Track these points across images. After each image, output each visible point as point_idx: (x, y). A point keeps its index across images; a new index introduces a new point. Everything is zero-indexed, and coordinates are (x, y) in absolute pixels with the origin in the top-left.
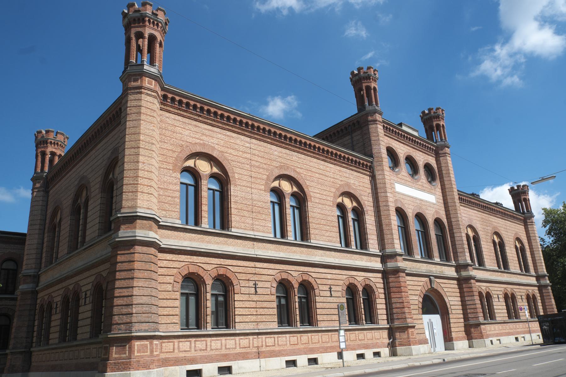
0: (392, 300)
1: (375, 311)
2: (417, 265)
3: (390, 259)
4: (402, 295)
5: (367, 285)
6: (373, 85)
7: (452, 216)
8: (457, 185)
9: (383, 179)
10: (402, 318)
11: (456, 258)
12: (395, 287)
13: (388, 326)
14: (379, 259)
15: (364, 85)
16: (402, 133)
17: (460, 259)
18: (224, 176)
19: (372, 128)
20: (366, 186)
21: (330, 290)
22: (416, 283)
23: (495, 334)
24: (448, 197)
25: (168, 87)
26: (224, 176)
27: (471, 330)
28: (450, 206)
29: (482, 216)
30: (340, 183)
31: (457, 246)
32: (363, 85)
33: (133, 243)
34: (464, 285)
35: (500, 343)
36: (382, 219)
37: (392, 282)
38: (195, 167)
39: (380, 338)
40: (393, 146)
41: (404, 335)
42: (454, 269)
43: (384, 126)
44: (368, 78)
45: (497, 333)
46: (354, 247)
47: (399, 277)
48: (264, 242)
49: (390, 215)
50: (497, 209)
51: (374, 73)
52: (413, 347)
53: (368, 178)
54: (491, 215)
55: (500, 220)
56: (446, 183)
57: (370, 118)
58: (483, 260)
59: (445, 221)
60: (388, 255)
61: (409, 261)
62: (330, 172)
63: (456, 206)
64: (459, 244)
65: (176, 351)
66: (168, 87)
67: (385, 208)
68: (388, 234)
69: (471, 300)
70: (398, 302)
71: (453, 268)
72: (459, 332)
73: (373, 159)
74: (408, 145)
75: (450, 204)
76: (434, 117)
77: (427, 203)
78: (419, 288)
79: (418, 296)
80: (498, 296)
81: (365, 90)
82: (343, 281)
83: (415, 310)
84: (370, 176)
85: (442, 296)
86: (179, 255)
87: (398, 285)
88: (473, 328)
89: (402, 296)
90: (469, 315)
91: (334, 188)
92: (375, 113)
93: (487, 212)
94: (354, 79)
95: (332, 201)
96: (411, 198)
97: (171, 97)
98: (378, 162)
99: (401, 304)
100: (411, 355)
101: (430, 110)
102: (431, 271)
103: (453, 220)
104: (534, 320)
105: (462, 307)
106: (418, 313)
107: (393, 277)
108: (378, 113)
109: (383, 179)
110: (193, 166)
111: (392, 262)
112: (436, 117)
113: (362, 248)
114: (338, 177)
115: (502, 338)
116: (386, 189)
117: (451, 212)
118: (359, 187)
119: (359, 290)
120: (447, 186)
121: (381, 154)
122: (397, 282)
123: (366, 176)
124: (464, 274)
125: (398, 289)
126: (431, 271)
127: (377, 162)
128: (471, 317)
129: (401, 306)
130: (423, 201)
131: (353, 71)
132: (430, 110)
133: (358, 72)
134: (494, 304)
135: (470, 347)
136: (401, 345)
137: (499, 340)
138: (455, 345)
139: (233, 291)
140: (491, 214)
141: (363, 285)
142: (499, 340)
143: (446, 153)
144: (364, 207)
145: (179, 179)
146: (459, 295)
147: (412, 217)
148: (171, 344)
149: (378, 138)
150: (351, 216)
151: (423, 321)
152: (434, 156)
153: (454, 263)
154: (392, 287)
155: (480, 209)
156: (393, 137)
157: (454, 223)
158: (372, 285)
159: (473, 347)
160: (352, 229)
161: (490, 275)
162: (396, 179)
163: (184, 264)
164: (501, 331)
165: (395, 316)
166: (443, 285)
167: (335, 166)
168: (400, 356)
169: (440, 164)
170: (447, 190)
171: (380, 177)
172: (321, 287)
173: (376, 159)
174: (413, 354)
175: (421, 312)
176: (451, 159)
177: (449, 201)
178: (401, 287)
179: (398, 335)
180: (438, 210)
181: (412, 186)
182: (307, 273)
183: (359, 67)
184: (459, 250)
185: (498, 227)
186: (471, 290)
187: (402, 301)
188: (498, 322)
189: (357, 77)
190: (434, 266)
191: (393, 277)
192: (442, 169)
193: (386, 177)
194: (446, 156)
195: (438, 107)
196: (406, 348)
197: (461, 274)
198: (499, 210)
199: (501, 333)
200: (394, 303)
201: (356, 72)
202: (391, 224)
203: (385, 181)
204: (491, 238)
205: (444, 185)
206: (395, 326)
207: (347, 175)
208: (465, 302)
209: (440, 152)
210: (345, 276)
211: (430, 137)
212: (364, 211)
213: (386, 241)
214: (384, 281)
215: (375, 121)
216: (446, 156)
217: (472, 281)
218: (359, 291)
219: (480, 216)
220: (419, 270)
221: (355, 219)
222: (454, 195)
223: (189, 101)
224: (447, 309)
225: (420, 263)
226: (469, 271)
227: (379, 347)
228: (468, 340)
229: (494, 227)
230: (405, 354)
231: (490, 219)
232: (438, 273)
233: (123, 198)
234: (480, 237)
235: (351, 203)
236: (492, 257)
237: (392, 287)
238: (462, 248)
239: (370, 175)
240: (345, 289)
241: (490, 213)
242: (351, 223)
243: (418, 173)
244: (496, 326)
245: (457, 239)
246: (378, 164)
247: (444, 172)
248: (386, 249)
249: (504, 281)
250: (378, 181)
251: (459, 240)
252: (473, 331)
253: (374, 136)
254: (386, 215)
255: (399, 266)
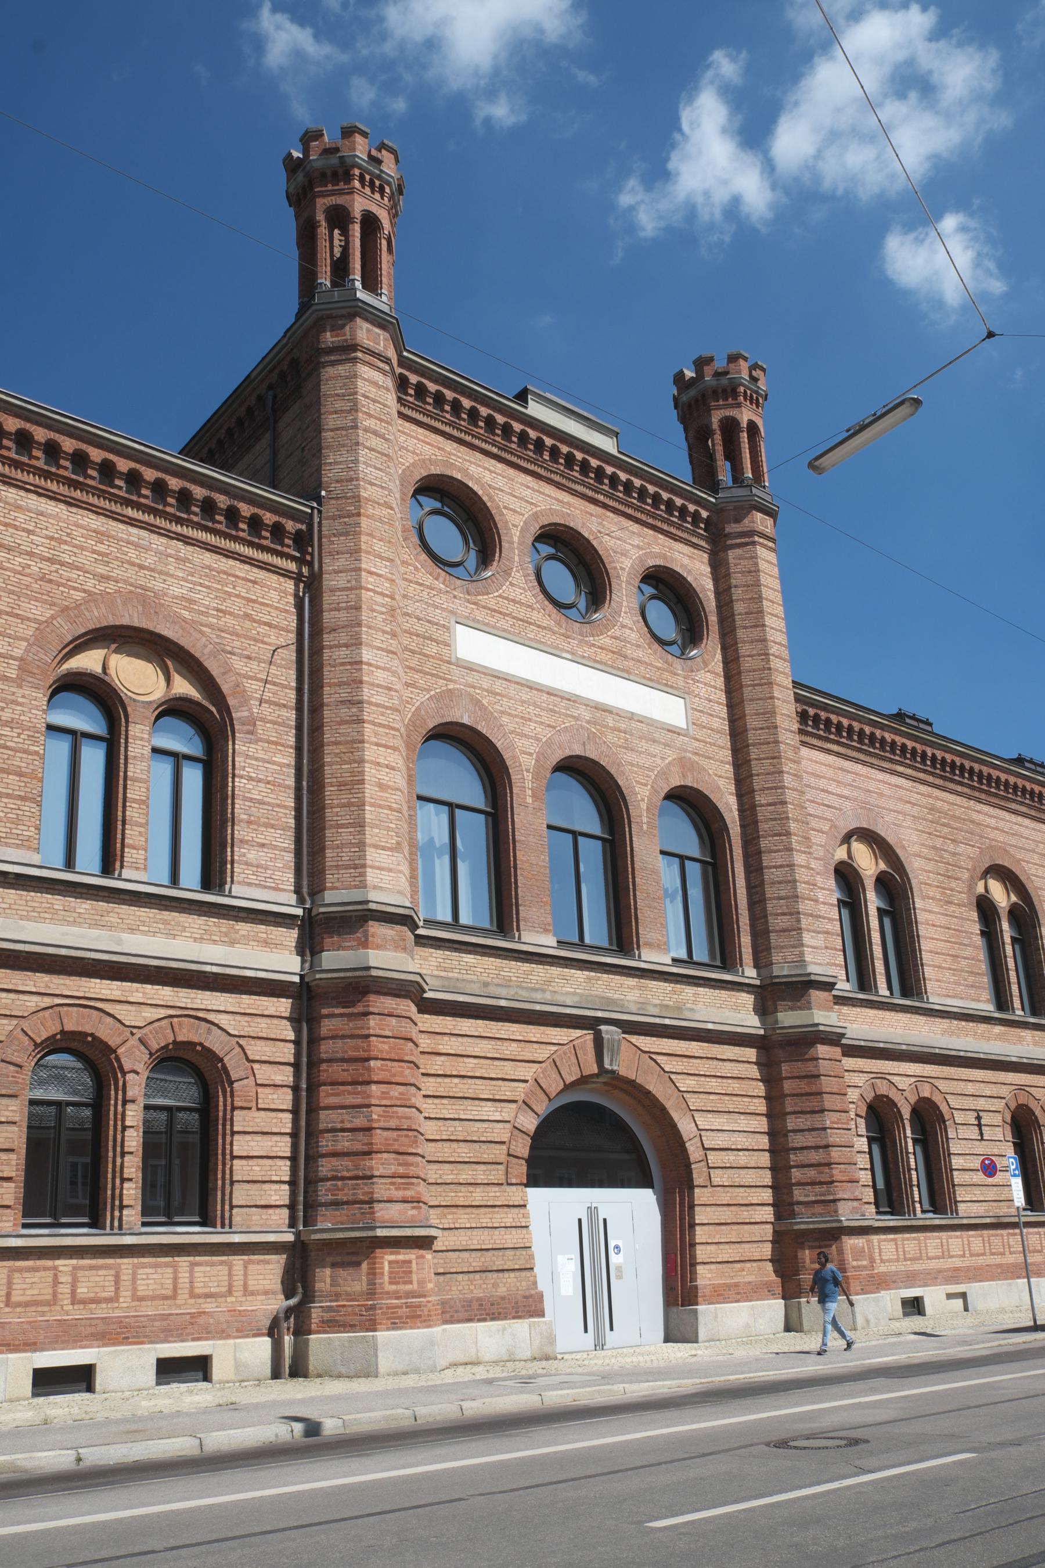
0: (318, 1119)
1: (224, 1164)
2: (527, 974)
3: (339, 934)
4: (369, 1096)
5: (1020, 1106)
6: (745, 415)
7: (757, 783)
8: (793, 661)
9: (350, 589)
10: (355, 1202)
11: (761, 957)
12: (343, 1060)
13: (290, 1237)
14: (290, 936)
15: (716, 418)
16: (575, 452)
17: (776, 957)
18: (213, 709)
19: (336, 378)
20: (267, 618)
21: (979, 1121)
22: (510, 1050)
23: (940, 1271)
24: (749, 708)
25: (142, 448)
26: (213, 709)
27: (800, 1254)
28: (754, 745)
29: (931, 801)
30: (90, 584)
31: (769, 906)
32: (318, 206)
33: (816, 1036)
34: (785, 1069)
35: (966, 1309)
36: (327, 759)
37: (333, 1037)
38: (102, 676)
39: (230, 1292)
40: (472, 478)
41: (355, 1282)
42: (747, 999)
43: (402, 384)
44: (730, 392)
45: (956, 1270)
46: (883, 990)
47: (367, 1014)
48: (262, 922)
49: (362, 742)
50: (1012, 780)
51: (751, 376)
52: (382, 1336)
53: (289, 585)
54: (979, 801)
55: (1027, 822)
56: (744, 649)
57: (329, 338)
58: (917, 971)
59: (728, 803)
60: (329, 918)
61: (484, 954)
62: (29, 532)
63: (777, 742)
64: (780, 898)
65: (125, 1294)
66: (142, 448)
67: (344, 712)
68: (342, 826)
69: (809, 1130)
70: (349, 1126)
71: (744, 995)
72: (738, 1266)
73: (320, 504)
74: (559, 486)
75: (752, 737)
76: (715, 392)
77: (634, 724)
78: (528, 1072)
79: (513, 1106)
80: (979, 1118)
81: (718, 432)
82: (858, 1090)
83: (482, 1167)
84: (298, 578)
85: (663, 1110)
86: (93, 980)
87: (357, 1049)
88: (811, 1248)
89: (366, 1102)
90: (796, 1192)
91: (45, 602)
92: (352, 316)
93: (959, 788)
94: (684, 398)
95: (21, 659)
96: (545, 696)
97: (152, 480)
98: (340, 517)
99: (360, 1136)
100: (369, 1372)
101: (700, 364)
102: (608, 1003)
103: (761, 799)
104: (909, 1223)
105: (773, 1159)
106: (502, 1179)
107: (342, 1015)
108: (366, 320)
109: (350, 589)
110: (98, 669)
111: (344, 949)
112: (724, 391)
113: (905, 993)
114: (85, 559)
115: (974, 1289)
116: (359, 633)
117: (756, 768)
118: (219, 618)
119: (121, 1067)
120: (746, 664)
121: (357, 487)
122: (352, 1037)
123: (275, 577)
124: (788, 1018)
125: (352, 1067)
126: (610, 1001)
127: (334, 518)
128: (802, 1199)
129: (359, 1147)
130: (611, 712)
131: (682, 372)
132: (700, 364)
133: (696, 373)
134: (953, 1150)
135: (788, 1329)
136: (332, 1325)
137: (963, 1296)
138: (702, 1320)
139: (120, 1093)
140: (983, 796)
141: (913, 1099)
142: (963, 1296)
143: (752, 533)
144: (231, 702)
145: (149, 741)
146: (763, 1109)
147: (536, 777)
148: (224, 1270)
149: (355, 420)
150: (873, 901)
151: (526, 1216)
152: (703, 543)
153: (750, 974)
154: (330, 1061)
155: (925, 771)
156: (477, 442)
157: (762, 813)
158: (216, 1048)
159: (801, 1331)
160: (876, 937)
161: (944, 1032)
162: (464, 609)
163: (163, 1012)
164: (981, 1261)
165: (324, 1192)
166: (669, 1065)
167: (74, 510)
168: (319, 1376)
169: (728, 575)
170: (746, 680)
171: (341, 581)
172: (959, 1117)
173: (330, 508)
174: (382, 1368)
175: (520, 1170)
176: (778, 559)
177: (752, 722)
178: (368, 1059)
179: (324, 1278)
180: (696, 758)
181: (557, 648)
182: (888, 1077)
183: (700, 357)
184: (777, 922)
185: (1011, 850)
186: (814, 1089)
187: (366, 1124)
188: (965, 1221)
189: (692, 392)
190: (631, 982)
191: (342, 1015)
192: (731, 596)
193: (368, 581)
194: (754, 543)
195: (733, 350)
196: (350, 1340)
197: (776, 1022)
198: (1020, 782)
199: (980, 1268)
200: (328, 1131)
201: (689, 374)
202: (362, 782)
203: (359, 598)
204: (971, 887)
205: (737, 659)
206: (796, 1227)
207: (150, 560)
208: (786, 1136)
209: (727, 530)
210: (35, 998)
211: (705, 475)
212: (231, 720)
213: (329, 853)
214: (298, 1031)
215: (349, 350)
216: (754, 543)
217: (823, 1050)
218: (124, 1074)
219: (924, 801)
220: (538, 996)
221: (884, 910)
222: (772, 698)
223: (112, 457)
224: (688, 1165)
225: (552, 964)
226: (810, 1008)
227: (206, 1334)
228: (783, 1298)
229: (991, 847)
230: (343, 1370)
231: (975, 816)
232: (655, 1011)
233: (327, 864)
234: (914, 882)
235: (873, 860)
236: (964, 962)
237: (330, 1061)
238: (791, 914)
239: (300, 574)
240: (863, 1114)
241: (977, 794)
242: (874, 923)
243: (603, 602)
244: (955, 1241)
245: (769, 875)
246: (337, 525)
247: (739, 607)
248: (324, 889)
249: (1014, 1059)
250: (328, 600)
251: (780, 883)
252: (808, 1261)
253: (336, 412)
254: (347, 742)
255: (816, 1022)
